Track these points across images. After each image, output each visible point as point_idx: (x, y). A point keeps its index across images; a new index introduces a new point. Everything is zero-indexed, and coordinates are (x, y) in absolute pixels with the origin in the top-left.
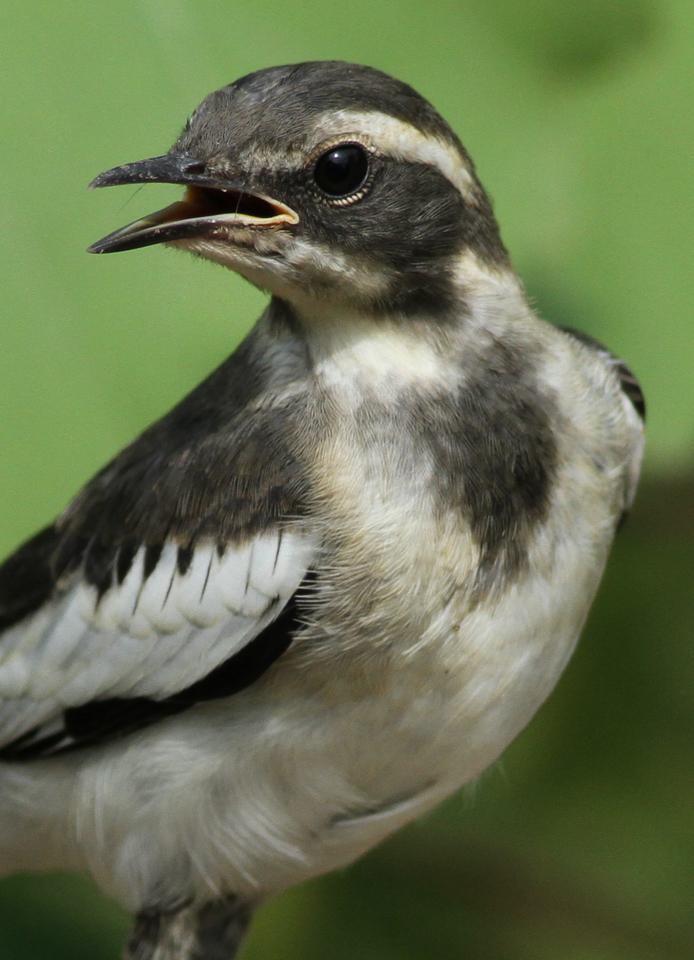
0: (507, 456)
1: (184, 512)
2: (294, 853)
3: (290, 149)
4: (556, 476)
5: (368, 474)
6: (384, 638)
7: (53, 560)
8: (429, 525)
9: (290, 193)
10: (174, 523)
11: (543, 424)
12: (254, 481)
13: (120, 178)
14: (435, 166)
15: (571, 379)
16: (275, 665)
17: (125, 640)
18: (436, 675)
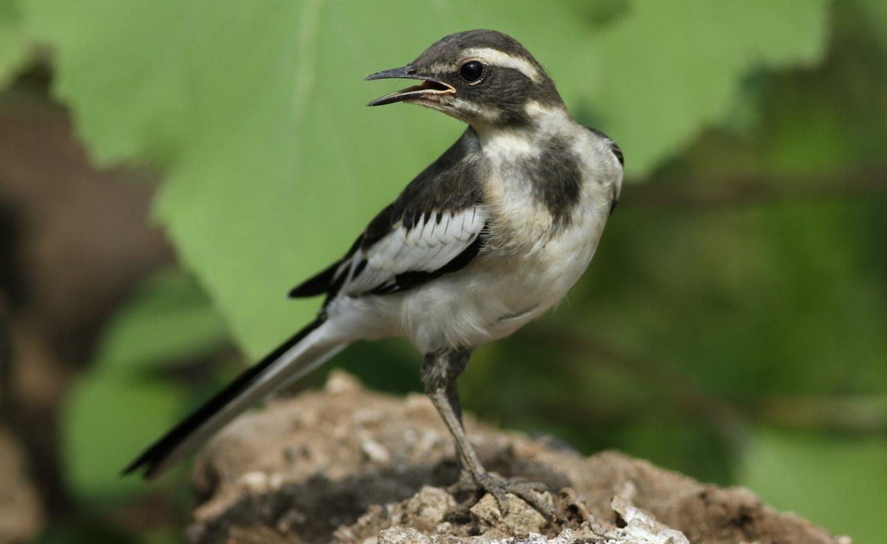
0: (561, 181)
1: (438, 200)
2: (484, 332)
3: (450, 64)
4: (582, 186)
5: (506, 190)
6: (515, 251)
8: (530, 209)
9: (452, 81)
10: (435, 204)
11: (575, 166)
13: (377, 77)
14: (517, 69)
15: (588, 150)
16: (473, 260)
17: (417, 248)
18: (537, 264)
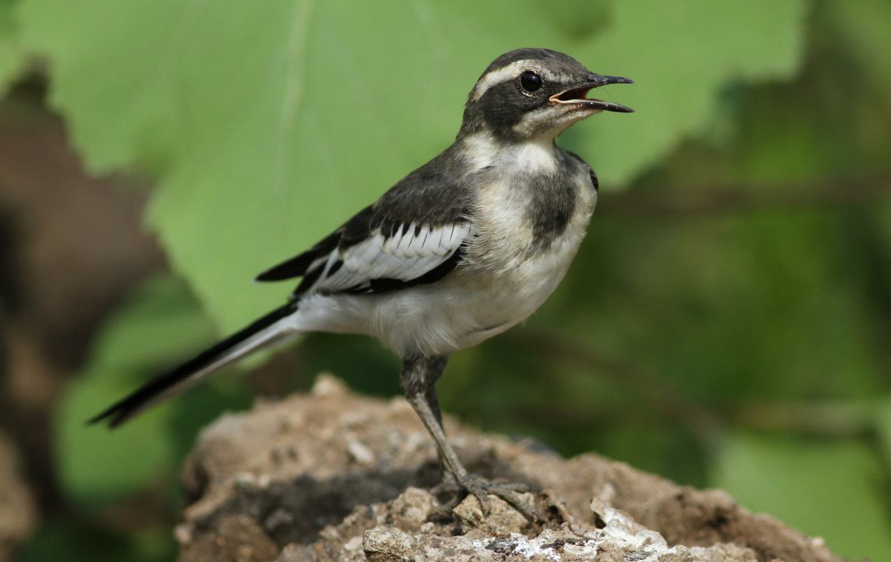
6: (490, 266)
7: (371, 221)
10: (415, 216)
12: (447, 204)
17: (393, 258)
18: (508, 282)
